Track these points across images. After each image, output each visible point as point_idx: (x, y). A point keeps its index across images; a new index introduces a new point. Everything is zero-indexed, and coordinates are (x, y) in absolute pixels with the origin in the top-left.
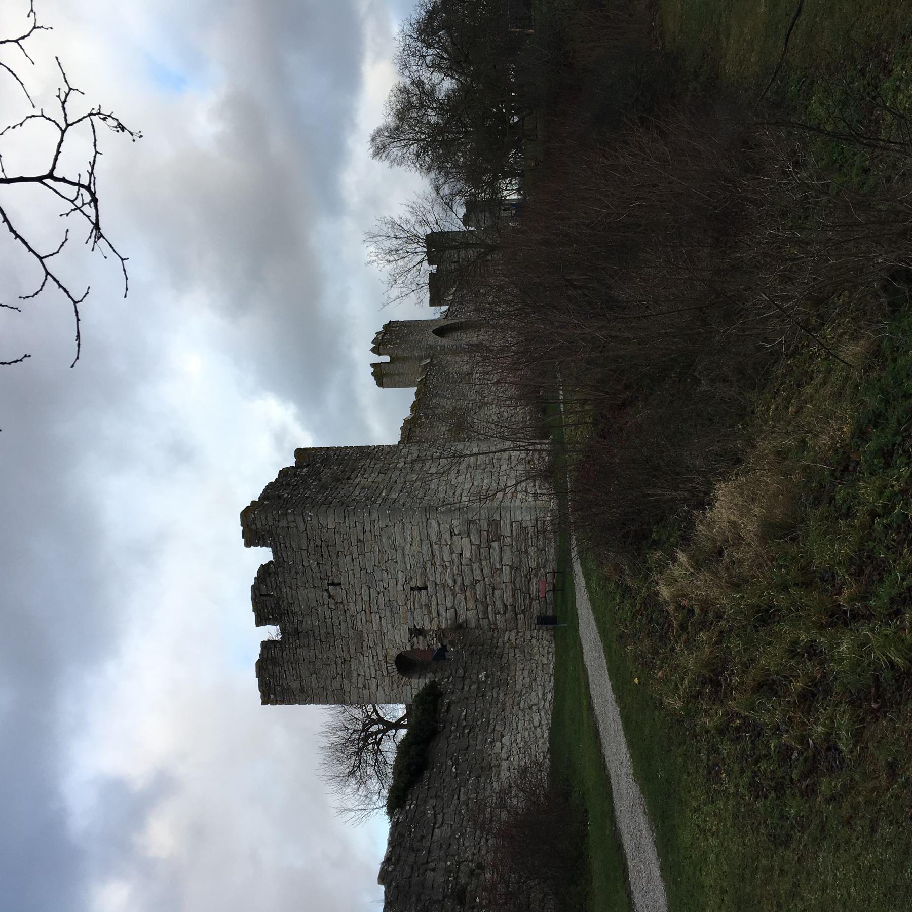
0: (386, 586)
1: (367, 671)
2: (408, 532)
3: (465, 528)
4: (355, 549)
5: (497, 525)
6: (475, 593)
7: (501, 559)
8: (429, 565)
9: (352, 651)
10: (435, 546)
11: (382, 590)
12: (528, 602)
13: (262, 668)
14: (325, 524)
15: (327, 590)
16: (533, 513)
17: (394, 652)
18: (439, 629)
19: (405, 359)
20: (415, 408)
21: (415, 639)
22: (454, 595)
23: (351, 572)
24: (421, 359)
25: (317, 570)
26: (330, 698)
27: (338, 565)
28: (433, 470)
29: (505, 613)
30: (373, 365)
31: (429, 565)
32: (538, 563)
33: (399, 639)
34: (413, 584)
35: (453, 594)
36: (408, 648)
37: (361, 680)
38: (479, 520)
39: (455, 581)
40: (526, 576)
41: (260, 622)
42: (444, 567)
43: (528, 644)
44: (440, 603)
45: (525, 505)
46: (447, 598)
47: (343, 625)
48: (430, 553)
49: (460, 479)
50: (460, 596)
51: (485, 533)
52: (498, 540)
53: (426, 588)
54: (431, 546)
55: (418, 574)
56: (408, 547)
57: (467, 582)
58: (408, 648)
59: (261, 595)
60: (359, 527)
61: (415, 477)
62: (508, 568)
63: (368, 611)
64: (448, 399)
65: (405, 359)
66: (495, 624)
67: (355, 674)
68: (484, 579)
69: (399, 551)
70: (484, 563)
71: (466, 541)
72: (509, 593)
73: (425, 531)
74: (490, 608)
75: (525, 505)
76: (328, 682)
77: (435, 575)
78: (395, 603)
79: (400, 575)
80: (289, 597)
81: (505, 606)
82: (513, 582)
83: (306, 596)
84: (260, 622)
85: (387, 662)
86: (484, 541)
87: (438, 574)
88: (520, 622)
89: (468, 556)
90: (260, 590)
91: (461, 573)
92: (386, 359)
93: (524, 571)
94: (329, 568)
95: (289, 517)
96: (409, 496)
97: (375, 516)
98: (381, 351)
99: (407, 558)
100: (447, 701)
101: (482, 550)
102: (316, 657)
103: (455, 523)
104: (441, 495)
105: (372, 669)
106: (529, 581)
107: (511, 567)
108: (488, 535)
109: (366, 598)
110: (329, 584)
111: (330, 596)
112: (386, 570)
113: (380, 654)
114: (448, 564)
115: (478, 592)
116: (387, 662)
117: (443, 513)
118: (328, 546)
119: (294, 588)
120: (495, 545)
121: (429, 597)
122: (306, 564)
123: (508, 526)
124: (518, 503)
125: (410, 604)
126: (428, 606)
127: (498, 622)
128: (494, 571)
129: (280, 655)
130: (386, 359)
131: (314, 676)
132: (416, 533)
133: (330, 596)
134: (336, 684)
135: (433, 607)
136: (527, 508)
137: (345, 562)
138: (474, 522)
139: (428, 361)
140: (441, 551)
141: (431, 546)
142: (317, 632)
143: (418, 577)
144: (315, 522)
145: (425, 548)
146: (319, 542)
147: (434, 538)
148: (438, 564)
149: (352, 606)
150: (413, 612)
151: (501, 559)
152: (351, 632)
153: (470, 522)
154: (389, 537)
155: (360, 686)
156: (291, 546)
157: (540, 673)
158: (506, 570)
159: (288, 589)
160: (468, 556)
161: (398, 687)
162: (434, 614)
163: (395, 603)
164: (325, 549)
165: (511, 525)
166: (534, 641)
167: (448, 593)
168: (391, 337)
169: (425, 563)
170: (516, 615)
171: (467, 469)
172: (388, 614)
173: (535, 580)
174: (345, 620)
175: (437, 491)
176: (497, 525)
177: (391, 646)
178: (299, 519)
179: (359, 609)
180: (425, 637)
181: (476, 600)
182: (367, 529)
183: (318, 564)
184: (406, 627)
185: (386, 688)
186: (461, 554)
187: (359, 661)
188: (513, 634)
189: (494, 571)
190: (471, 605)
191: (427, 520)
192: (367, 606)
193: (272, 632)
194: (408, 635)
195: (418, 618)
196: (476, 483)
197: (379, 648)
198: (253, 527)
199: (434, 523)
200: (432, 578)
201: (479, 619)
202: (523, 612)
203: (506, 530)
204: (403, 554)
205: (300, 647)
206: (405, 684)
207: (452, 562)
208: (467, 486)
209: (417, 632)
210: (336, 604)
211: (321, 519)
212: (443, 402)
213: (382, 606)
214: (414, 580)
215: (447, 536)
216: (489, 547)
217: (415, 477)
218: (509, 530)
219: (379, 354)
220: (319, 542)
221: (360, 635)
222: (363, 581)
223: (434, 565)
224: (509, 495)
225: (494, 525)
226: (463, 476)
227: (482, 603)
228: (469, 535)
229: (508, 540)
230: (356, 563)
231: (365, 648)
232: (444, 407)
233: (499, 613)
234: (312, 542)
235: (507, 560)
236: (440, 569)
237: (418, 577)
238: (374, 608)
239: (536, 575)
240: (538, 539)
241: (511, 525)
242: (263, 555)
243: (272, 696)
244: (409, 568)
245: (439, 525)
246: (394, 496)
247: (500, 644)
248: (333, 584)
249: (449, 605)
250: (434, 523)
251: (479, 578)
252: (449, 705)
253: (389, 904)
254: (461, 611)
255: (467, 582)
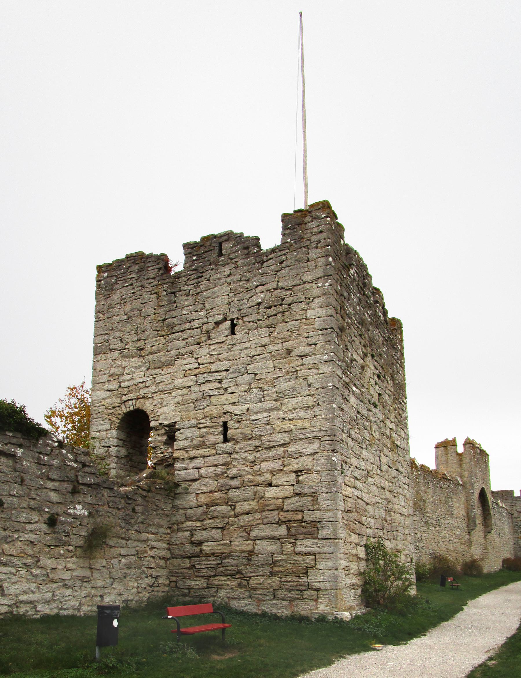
0: (229, 390)
1: (128, 377)
2: (302, 414)
3: (306, 490)
4: (278, 347)
5: (310, 534)
6: (217, 505)
7: (263, 538)
8: (256, 443)
9: (151, 357)
10: (281, 450)
11: (225, 386)
12: (205, 573)
13: (138, 260)
14: (312, 305)
15: (225, 320)
16: (328, 585)
17: (148, 406)
18: (175, 459)
19: (460, 464)
20: (423, 467)
21: (163, 431)
22: (217, 477)
23: (247, 345)
24: (461, 477)
25: (251, 304)
26: (101, 338)
27: (257, 328)
28: (384, 459)
29: (192, 543)
30: (454, 440)
31: (256, 443)
32: (255, 589)
33: (163, 411)
34: (231, 424)
35: (217, 476)
36: (152, 424)
37: (118, 371)
38: (318, 510)
39: (234, 478)
40: (239, 572)
41: (190, 248)
42: (253, 463)
43: (144, 572)
44: (207, 459)
45: (341, 573)
46: (212, 469)
47: (180, 343)
48: (272, 444)
49: (373, 488)
50: (214, 484)
51: (299, 517)
52: (290, 535)
53: (226, 440)
54: (282, 445)
55: (243, 431)
56: (281, 414)
57: (233, 493)
58: (152, 424)
59: (220, 244)
60: (308, 350)
61: (376, 435)
62: (250, 548)
63: (197, 371)
64: (432, 497)
65: (460, 464)
66: (179, 530)
67: (124, 363)
68: (236, 516)
69: (277, 404)
70: (258, 516)
71: (288, 491)
72: (218, 549)
73: (302, 436)
74: (198, 524)
75: (341, 573)
76: (118, 334)
77: (243, 453)
78: (208, 402)
79: (243, 407)
80: (218, 276)
81: (200, 544)
82: (231, 555)
83: (220, 296)
84: (190, 248)
85: (137, 399)
86: (289, 516)
87: (243, 455)
88: (179, 561)
89: (268, 495)
90: (227, 241)
91: (244, 485)
92: (460, 449)
93: (245, 570)
94: (254, 317)
95: (323, 259)
96: (352, 419)
97: (325, 368)
98: (467, 446)
99: (265, 414)
100: (19, 452)
101: (275, 513)
102: (146, 317)
103: (314, 476)
104: (354, 461)
105: (131, 382)
106: (232, 576)
107: (251, 552)
108: (296, 521)
109: (214, 368)
110: (232, 320)
111: (218, 324)
112: (250, 389)
113: (146, 391)
114: (256, 468)
115: (219, 508)
116: (137, 399)
117: (329, 459)
118: (283, 313)
119: (229, 279)
120: (282, 531)
121: (215, 444)
122: (258, 289)
123: (308, 550)
124: (343, 563)
125: (206, 422)
126: (202, 445)
127: (180, 534)
128: (247, 530)
129: (150, 276)
130: (460, 449)
131: (125, 317)
132: (300, 424)
133: (218, 324)
134: (115, 344)
135: (201, 452)
136: (336, 577)
137: (260, 336)
138: (315, 501)
139: (461, 483)
140: (274, 459)
141: (282, 445)
142: (174, 313)
143: (239, 431)
144: (315, 292)
145: (280, 438)
146: (288, 301)
147: (292, 448)
148: (257, 455)
149: (204, 351)
150: (195, 426)
151: (263, 538)
152: (174, 353)
153: (314, 495)
154: (294, 389)
155: (112, 371)
156: (282, 268)
157: (84, 593)
158: (247, 546)
159: (227, 273)
160: (268, 495)
161: (110, 414)
162: (193, 453)
163: (208, 402)
164: (280, 309)
165: (310, 554)
166: (149, 581)
167: (219, 470)
168: (477, 454)
169: (259, 437)
170: (189, 558)
171: (386, 499)
172: (193, 396)
173: (233, 583)
174: (188, 345)
175: (358, 457)
176: (310, 534)
177: (155, 402)
178: (319, 272)
179: (200, 360)
180: (165, 443)
181: (209, 505)
182: (306, 360)
183: (259, 304)
184: (177, 419)
185: (108, 401)
186: (270, 485)
187: (140, 367)
188: (163, 553)
189: (247, 530)
190: (203, 499)
191: (319, 438)
192: (206, 370)
193: (178, 261)
194: (167, 422)
195: (188, 433)
196: (369, 508)
197: (153, 388)
198: (309, 218)
199: (313, 447)
200: (238, 447)
201: (185, 509)
202: (193, 567)
203: (304, 545)
204: (270, 410)
205: (158, 298)
206: (112, 422)
207: (259, 473)
208: (366, 497)
209: (171, 433)
210: (208, 332)
211: (320, 300)
212: (430, 492)
213: (203, 387)
214: (237, 425)
215: (296, 464)
216: (279, 523)
217: (376, 435)
218: (304, 550)
219: (465, 444)
220: (288, 301)
221: (170, 364)
222: (236, 362)
223: (256, 449)
224: (354, 551)
225: (313, 529)
226: (377, 493)
227: (206, 513)
228: (297, 495)
229: (288, 548)
230: (260, 350)
231: (154, 372)
232: (426, 492)
233: (192, 535)
234: (289, 292)
235: (263, 546)
236: (250, 457)
237: (239, 431)
238: (202, 379)
239: (240, 585)
240: (290, 590)
241: (310, 554)
242: (271, 238)
243: (105, 275)
244: (253, 417)
245: (312, 454)
246: (353, 400)
247: (144, 536)
248: (233, 326)
249: (203, 471)
250: (313, 447)
251: (238, 509)
252: (13, 456)
253: (519, 580)
254: (195, 486)
255: (233, 493)
